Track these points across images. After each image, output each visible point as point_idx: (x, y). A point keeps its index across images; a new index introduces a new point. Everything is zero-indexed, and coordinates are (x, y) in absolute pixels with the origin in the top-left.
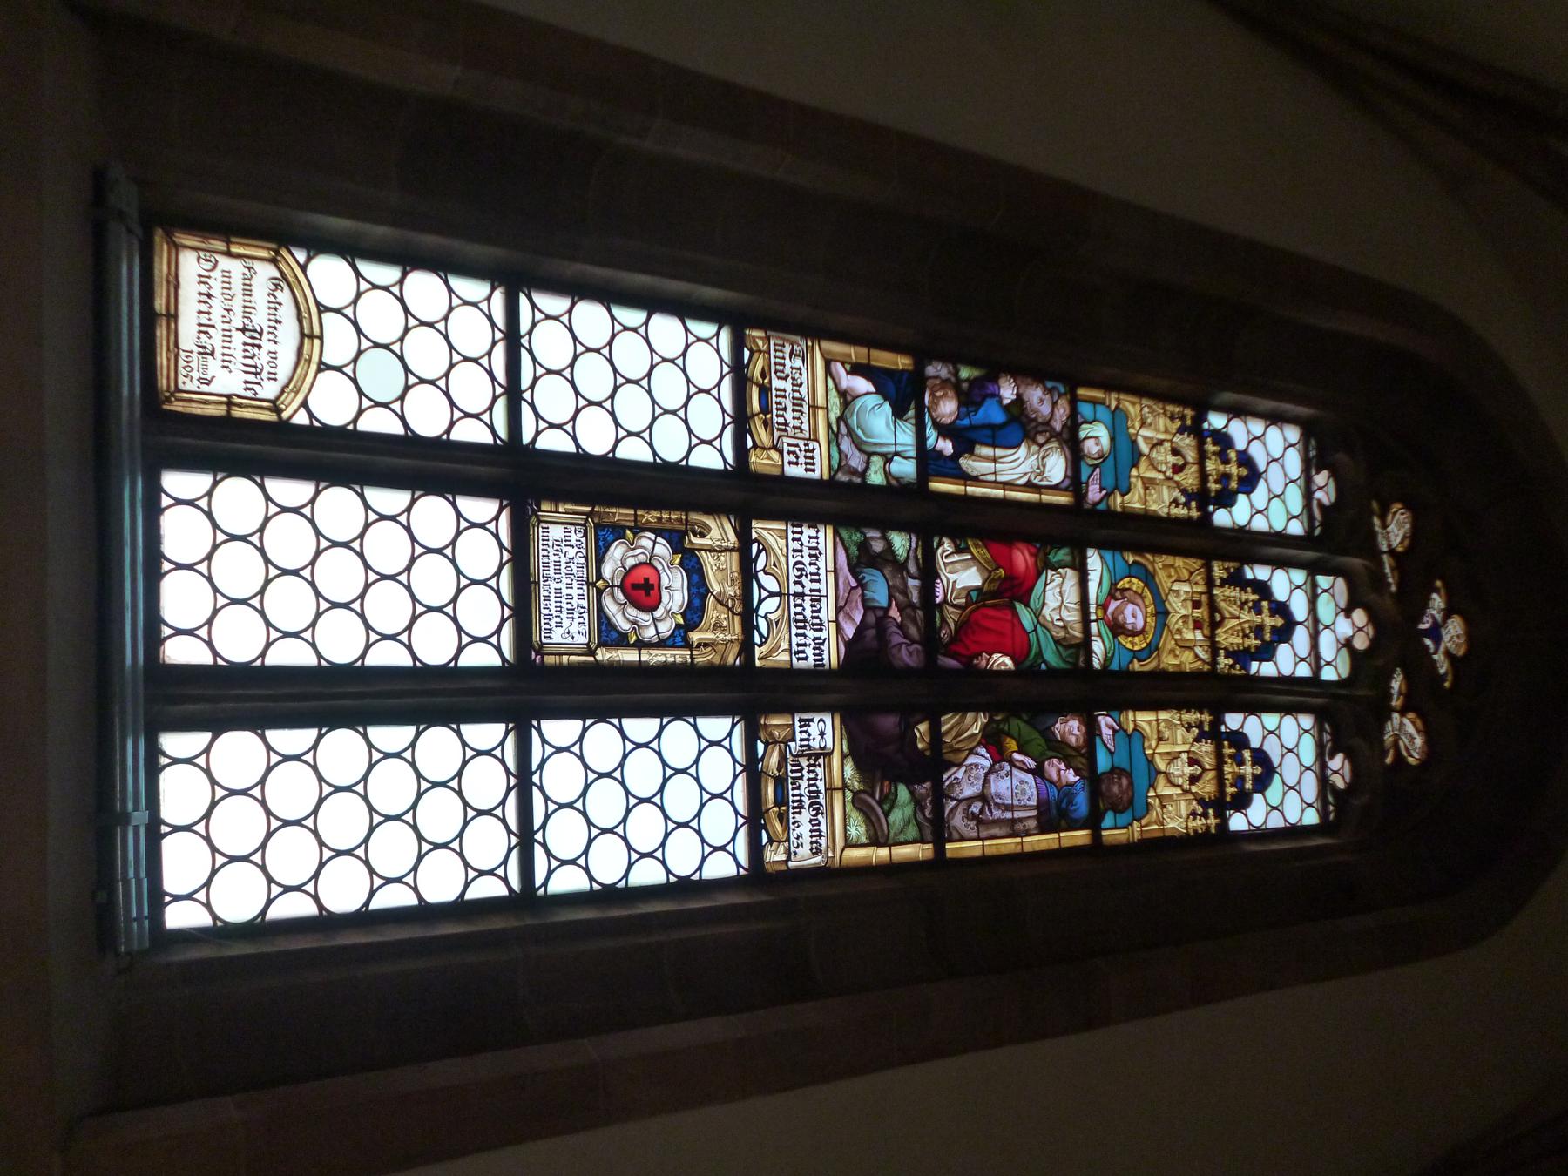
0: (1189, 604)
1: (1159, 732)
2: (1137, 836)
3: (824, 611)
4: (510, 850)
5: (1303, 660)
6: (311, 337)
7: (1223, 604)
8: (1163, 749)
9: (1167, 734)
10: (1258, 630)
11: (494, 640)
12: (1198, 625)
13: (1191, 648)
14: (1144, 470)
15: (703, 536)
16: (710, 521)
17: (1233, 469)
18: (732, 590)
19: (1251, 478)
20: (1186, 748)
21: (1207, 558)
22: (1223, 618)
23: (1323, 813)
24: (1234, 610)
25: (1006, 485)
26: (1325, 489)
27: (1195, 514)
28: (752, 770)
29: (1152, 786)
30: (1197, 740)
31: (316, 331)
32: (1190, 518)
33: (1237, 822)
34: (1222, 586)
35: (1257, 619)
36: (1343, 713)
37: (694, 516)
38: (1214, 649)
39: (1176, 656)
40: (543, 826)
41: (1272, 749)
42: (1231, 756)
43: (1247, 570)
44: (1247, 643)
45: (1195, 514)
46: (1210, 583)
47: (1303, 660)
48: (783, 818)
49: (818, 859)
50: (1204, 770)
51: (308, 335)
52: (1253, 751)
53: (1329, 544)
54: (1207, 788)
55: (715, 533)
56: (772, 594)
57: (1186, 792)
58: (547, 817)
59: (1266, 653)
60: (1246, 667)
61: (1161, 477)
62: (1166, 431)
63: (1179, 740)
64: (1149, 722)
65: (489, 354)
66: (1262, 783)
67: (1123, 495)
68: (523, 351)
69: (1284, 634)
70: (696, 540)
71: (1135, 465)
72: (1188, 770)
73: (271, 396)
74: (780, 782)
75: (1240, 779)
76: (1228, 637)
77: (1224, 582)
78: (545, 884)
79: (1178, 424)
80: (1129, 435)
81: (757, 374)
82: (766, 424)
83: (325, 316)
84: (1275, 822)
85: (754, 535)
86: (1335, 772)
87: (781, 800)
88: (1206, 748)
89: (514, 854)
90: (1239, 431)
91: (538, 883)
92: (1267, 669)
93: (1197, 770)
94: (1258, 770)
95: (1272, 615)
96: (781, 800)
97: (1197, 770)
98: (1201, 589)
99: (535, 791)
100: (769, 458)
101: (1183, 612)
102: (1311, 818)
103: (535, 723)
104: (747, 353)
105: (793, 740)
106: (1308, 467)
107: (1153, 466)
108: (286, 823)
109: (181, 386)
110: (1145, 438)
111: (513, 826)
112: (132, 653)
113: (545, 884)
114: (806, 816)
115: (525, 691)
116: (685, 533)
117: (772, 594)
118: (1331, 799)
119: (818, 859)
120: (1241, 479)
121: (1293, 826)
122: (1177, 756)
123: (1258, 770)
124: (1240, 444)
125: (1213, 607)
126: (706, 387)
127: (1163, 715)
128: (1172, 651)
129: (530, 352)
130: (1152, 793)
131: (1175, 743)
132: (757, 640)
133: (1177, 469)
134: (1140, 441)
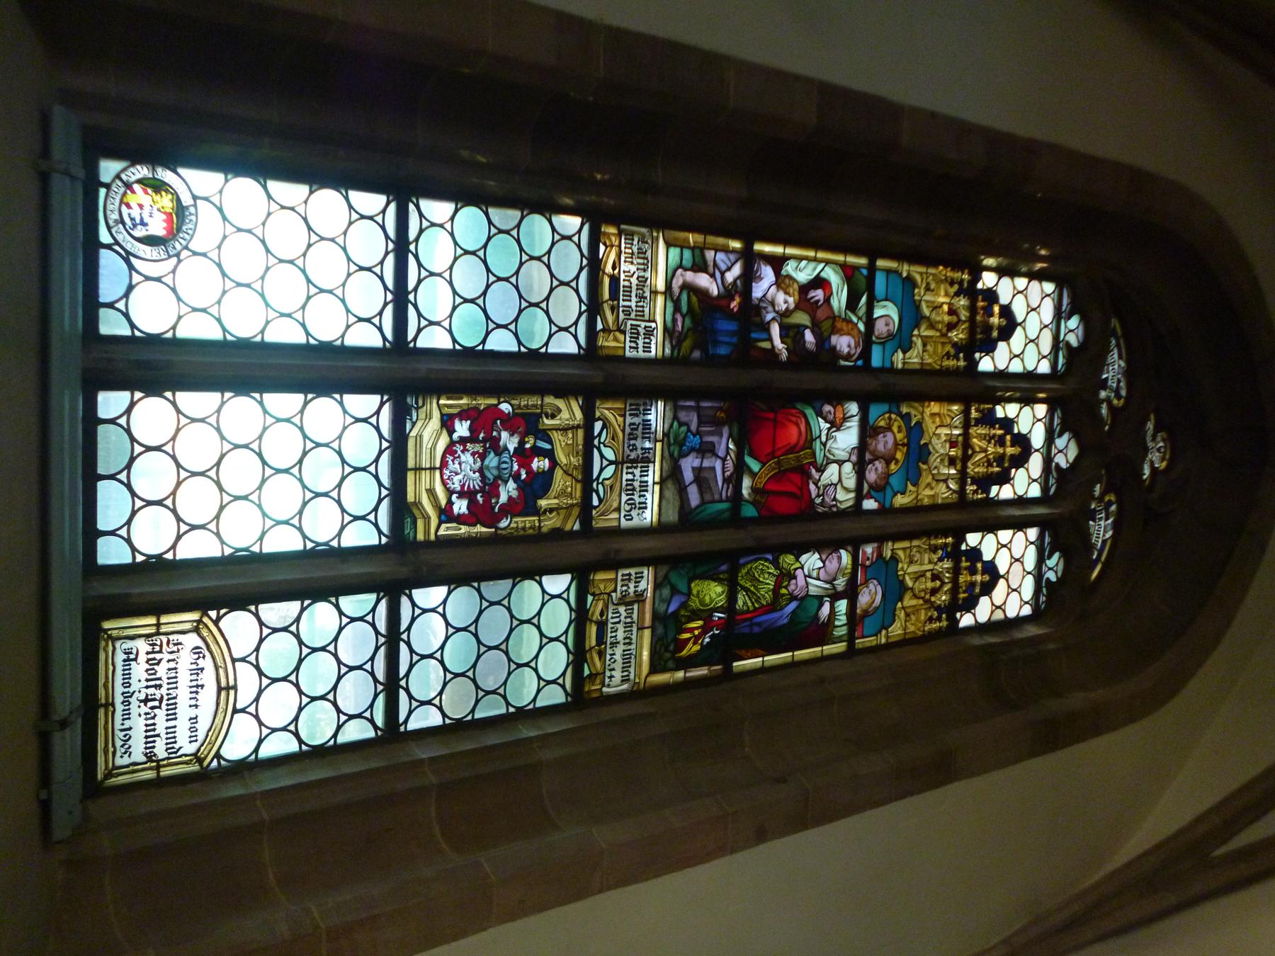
0: (948, 445)
1: (928, 284)
2: (883, 641)
3: (651, 473)
4: (386, 304)
5: (1034, 480)
6: (228, 688)
7: (975, 440)
8: (927, 297)
9: (933, 286)
10: (1000, 459)
11: (373, 420)
12: (952, 462)
13: (945, 481)
14: (909, 601)
15: (553, 416)
16: (560, 403)
17: (995, 320)
18: (576, 461)
19: (1010, 325)
20: (930, 567)
21: (966, 401)
22: (974, 452)
23: (1045, 489)
24: (983, 444)
25: (815, 259)
26: (1073, 328)
27: (962, 363)
28: (580, 617)
29: (901, 600)
30: (957, 294)
31: (231, 683)
32: (958, 367)
33: (966, 620)
34: (976, 425)
35: (1000, 450)
36: (1057, 520)
37: (549, 400)
38: (962, 477)
39: (932, 489)
40: (416, 289)
41: (1019, 310)
42: (966, 568)
43: (999, 409)
44: (991, 470)
45: (962, 363)
46: (966, 425)
47: (1034, 480)
48: (601, 654)
49: (625, 686)
50: (959, 320)
51: (227, 689)
52: (984, 563)
53: (1067, 390)
54: (958, 335)
55: (565, 415)
56: (611, 463)
57: (944, 335)
58: (420, 281)
59: (1004, 479)
60: (988, 491)
61: (921, 602)
62: (930, 562)
63: (926, 561)
64: (921, 274)
65: (382, 263)
66: (988, 589)
67: (904, 352)
68: (410, 256)
69: (1020, 461)
70: (547, 422)
71: (917, 326)
72: (947, 318)
73: (194, 636)
74: (602, 626)
75: (989, 328)
76: (976, 468)
77: (978, 422)
78: (415, 339)
79: (956, 287)
80: (915, 301)
81: (597, 616)
82: (612, 309)
83: (237, 664)
84: (1016, 367)
85: (598, 414)
86: (1050, 569)
87: (601, 638)
88: (963, 302)
89: (390, 308)
90: (1005, 289)
91: (410, 337)
92: (1006, 492)
93: (954, 319)
94: (987, 578)
95: (1012, 446)
96: (601, 638)
97: (954, 319)
98: (956, 432)
99: (410, 307)
100: (616, 339)
101: (942, 451)
102: (1044, 368)
103: (402, 729)
104: (602, 248)
105: (615, 591)
106: (1059, 315)
107: (932, 326)
108: (194, 527)
109: (118, 644)
110: (927, 302)
111: (390, 284)
112: (67, 317)
113: (415, 339)
114: (619, 651)
115: (395, 566)
116: (539, 416)
117: (611, 463)
118: (1044, 590)
119: (625, 686)
120: (1000, 328)
121: (1020, 497)
122: (923, 574)
123: (987, 578)
124: (1004, 300)
125: (967, 445)
126: (566, 280)
127: (915, 543)
128: (929, 485)
129: (416, 257)
130: (916, 332)
131: (921, 564)
132: (595, 502)
133: (951, 327)
134: (924, 305)
